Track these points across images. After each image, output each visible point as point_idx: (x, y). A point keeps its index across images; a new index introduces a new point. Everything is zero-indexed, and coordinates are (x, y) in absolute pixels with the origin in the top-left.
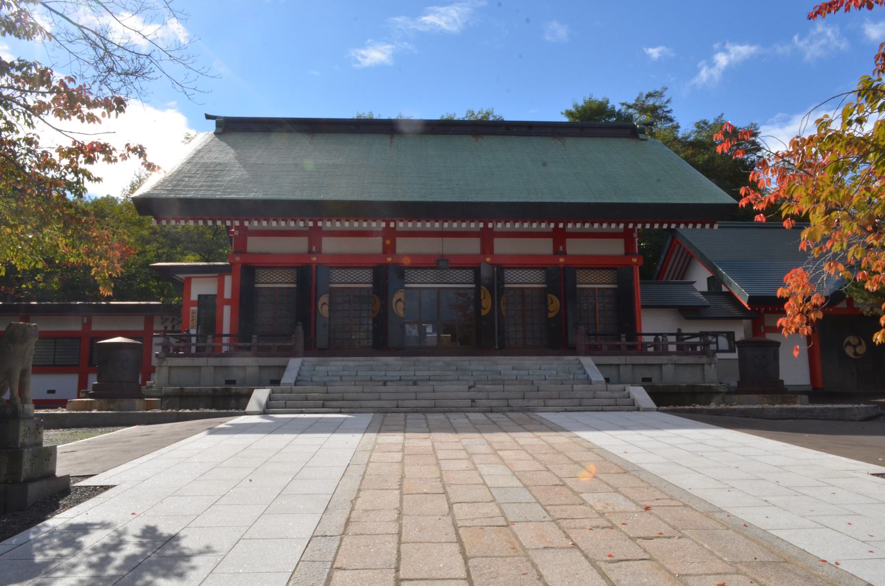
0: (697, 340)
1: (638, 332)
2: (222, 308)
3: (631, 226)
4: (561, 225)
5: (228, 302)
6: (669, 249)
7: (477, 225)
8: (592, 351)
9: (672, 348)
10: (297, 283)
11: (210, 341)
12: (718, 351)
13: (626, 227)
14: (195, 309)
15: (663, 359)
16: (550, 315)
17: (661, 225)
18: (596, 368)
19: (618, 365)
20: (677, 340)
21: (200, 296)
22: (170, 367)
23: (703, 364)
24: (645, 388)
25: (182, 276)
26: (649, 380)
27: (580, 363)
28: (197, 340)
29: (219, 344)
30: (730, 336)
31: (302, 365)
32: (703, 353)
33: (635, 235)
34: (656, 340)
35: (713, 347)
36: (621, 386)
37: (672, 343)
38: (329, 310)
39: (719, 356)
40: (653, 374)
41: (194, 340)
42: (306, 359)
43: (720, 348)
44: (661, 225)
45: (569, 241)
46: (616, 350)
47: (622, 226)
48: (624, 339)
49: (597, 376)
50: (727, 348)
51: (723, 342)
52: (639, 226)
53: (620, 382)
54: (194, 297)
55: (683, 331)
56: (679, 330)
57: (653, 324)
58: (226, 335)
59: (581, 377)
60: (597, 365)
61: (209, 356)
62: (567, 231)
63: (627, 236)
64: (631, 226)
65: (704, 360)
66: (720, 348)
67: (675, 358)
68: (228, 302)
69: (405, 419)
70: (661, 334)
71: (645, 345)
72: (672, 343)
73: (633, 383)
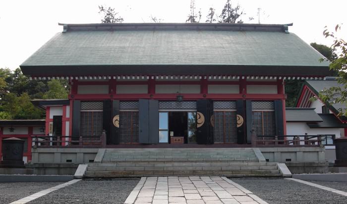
0: (316, 139)
1: (285, 135)
2: (65, 123)
3: (280, 78)
4: (243, 78)
5: (68, 119)
6: (302, 92)
7: (145, 78)
8: (260, 144)
9: (302, 143)
10: (104, 109)
11: (58, 140)
12: (327, 145)
13: (278, 79)
14: (52, 123)
15: (297, 149)
16: (238, 126)
17: (292, 78)
18: (261, 153)
19: (273, 152)
20: (305, 138)
21: (54, 116)
22: (39, 153)
23: (318, 152)
24: (286, 164)
25: (45, 106)
26: (290, 160)
27: (253, 151)
28: (53, 139)
29: (54, 141)
30: (333, 136)
31: (105, 152)
32: (318, 146)
33: (283, 83)
34: (294, 139)
35: (323, 143)
36: (274, 163)
37: (302, 141)
38: (119, 124)
39: (327, 147)
40: (291, 156)
41: (51, 139)
42: (107, 149)
43: (328, 143)
44: (292, 78)
45: (118, 86)
46: (272, 144)
47: (275, 78)
48: (277, 139)
49: (262, 158)
50: (332, 143)
51: (330, 141)
52: (285, 78)
53: (274, 161)
54: (51, 117)
55: (308, 134)
56: (306, 134)
57: (292, 131)
58: (67, 137)
59: (253, 159)
60: (262, 152)
61: (58, 147)
62: (156, 80)
63: (278, 84)
64: (280, 78)
65: (318, 149)
66: (328, 143)
67: (303, 149)
68: (68, 119)
69: (168, 179)
70: (296, 136)
71: (287, 142)
72: (302, 141)
73: (281, 162)
